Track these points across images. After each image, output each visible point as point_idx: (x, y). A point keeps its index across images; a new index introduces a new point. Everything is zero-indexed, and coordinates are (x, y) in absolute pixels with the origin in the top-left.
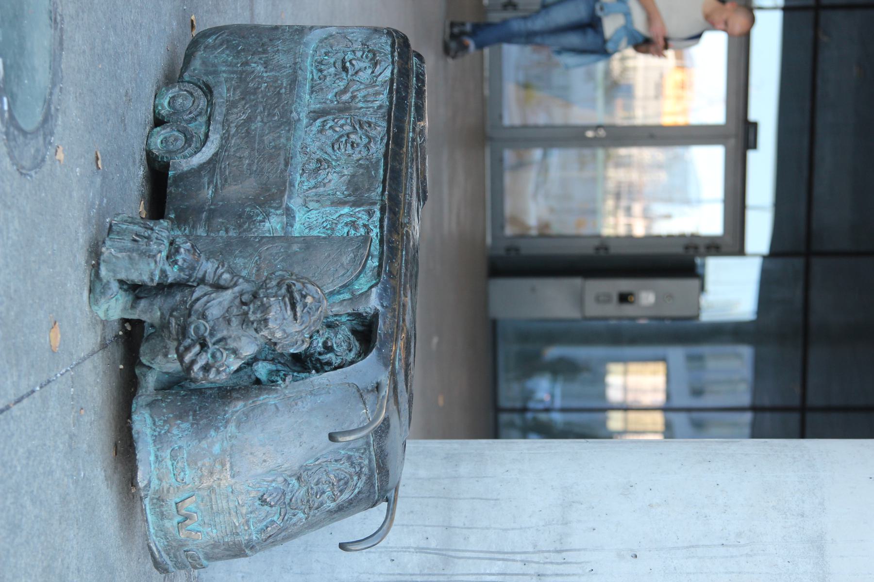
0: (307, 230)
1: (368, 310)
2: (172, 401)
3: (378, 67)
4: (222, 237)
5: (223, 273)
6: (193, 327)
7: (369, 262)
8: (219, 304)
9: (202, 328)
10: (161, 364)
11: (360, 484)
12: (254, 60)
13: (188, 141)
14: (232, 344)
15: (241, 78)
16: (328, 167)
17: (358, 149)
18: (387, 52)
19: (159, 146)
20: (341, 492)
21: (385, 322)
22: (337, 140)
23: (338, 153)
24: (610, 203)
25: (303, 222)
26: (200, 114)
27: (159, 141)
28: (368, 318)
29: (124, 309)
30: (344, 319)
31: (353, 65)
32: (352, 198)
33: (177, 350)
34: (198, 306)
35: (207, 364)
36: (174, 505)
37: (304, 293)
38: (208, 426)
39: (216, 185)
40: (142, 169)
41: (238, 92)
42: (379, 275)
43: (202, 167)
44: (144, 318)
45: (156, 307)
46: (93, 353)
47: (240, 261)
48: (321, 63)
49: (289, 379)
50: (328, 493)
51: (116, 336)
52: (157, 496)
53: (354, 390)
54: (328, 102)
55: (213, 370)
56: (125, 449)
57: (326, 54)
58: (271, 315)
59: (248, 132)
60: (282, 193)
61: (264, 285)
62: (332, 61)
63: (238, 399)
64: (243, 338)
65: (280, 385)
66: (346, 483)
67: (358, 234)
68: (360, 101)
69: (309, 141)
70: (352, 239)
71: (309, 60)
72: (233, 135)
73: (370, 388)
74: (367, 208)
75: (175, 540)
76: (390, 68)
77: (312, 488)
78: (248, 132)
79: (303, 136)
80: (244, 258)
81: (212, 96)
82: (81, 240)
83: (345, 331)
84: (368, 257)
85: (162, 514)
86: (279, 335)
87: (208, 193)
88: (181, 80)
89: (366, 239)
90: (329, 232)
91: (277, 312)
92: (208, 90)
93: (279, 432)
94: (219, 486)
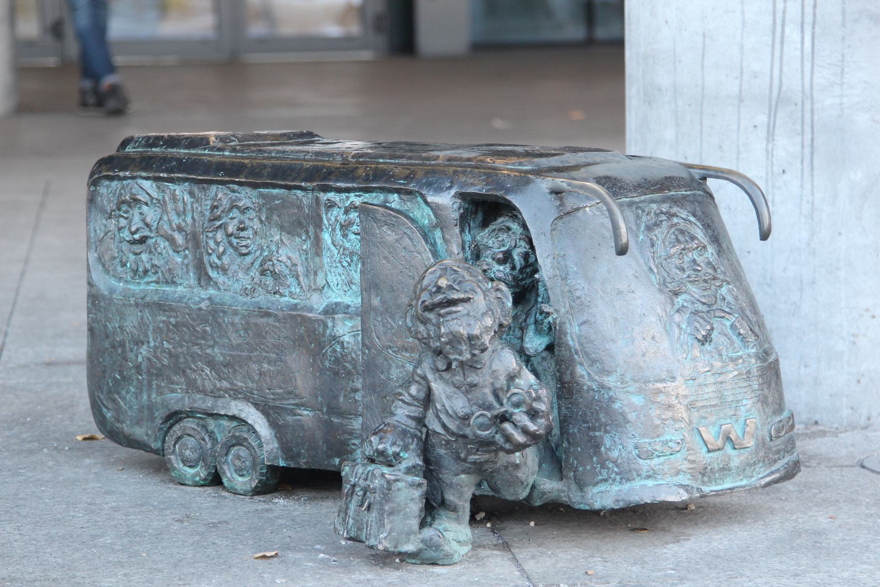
0: (354, 287)
1: (456, 206)
3: (139, 197)
4: (363, 397)
5: (410, 395)
6: (479, 432)
8: (450, 399)
9: (481, 420)
10: (529, 473)
11: (684, 214)
12: (134, 358)
13: (240, 442)
14: (502, 381)
15: (157, 375)
16: (270, 260)
17: (247, 222)
18: (119, 186)
20: (693, 238)
21: (472, 184)
22: (236, 249)
23: (253, 248)
25: (342, 293)
26: (204, 427)
27: (240, 479)
28: (467, 206)
29: (458, 520)
30: (468, 237)
32: (311, 229)
33: (509, 452)
34: (452, 426)
36: (711, 454)
37: (434, 290)
38: (608, 411)
39: (296, 405)
40: (276, 500)
41: (175, 378)
42: (410, 193)
43: (273, 424)
44: (468, 495)
45: (455, 480)
46: (515, 559)
48: (135, 272)
49: (546, 308)
50: (695, 255)
51: (493, 531)
52: (700, 476)
53: (560, 223)
54: (186, 261)
55: (535, 405)
56: (639, 518)
57: (124, 265)
58: (464, 331)
59: (227, 365)
60: (305, 320)
61: (424, 341)
62: (132, 257)
63: (573, 374)
64: (494, 367)
65: (555, 319)
66: (682, 232)
67: (358, 220)
68: (184, 220)
69: (237, 286)
70: (364, 229)
71: (132, 287)
72: (232, 384)
73: (558, 203)
74: (323, 209)
75: (756, 452)
76: (140, 181)
77: (689, 277)
78: (227, 365)
79: (230, 294)
83: (484, 237)
84: (387, 208)
85: (723, 469)
86: (489, 321)
88: (161, 452)
89: (364, 210)
90: (355, 258)
91: (460, 323)
93: (616, 320)
94: (686, 396)
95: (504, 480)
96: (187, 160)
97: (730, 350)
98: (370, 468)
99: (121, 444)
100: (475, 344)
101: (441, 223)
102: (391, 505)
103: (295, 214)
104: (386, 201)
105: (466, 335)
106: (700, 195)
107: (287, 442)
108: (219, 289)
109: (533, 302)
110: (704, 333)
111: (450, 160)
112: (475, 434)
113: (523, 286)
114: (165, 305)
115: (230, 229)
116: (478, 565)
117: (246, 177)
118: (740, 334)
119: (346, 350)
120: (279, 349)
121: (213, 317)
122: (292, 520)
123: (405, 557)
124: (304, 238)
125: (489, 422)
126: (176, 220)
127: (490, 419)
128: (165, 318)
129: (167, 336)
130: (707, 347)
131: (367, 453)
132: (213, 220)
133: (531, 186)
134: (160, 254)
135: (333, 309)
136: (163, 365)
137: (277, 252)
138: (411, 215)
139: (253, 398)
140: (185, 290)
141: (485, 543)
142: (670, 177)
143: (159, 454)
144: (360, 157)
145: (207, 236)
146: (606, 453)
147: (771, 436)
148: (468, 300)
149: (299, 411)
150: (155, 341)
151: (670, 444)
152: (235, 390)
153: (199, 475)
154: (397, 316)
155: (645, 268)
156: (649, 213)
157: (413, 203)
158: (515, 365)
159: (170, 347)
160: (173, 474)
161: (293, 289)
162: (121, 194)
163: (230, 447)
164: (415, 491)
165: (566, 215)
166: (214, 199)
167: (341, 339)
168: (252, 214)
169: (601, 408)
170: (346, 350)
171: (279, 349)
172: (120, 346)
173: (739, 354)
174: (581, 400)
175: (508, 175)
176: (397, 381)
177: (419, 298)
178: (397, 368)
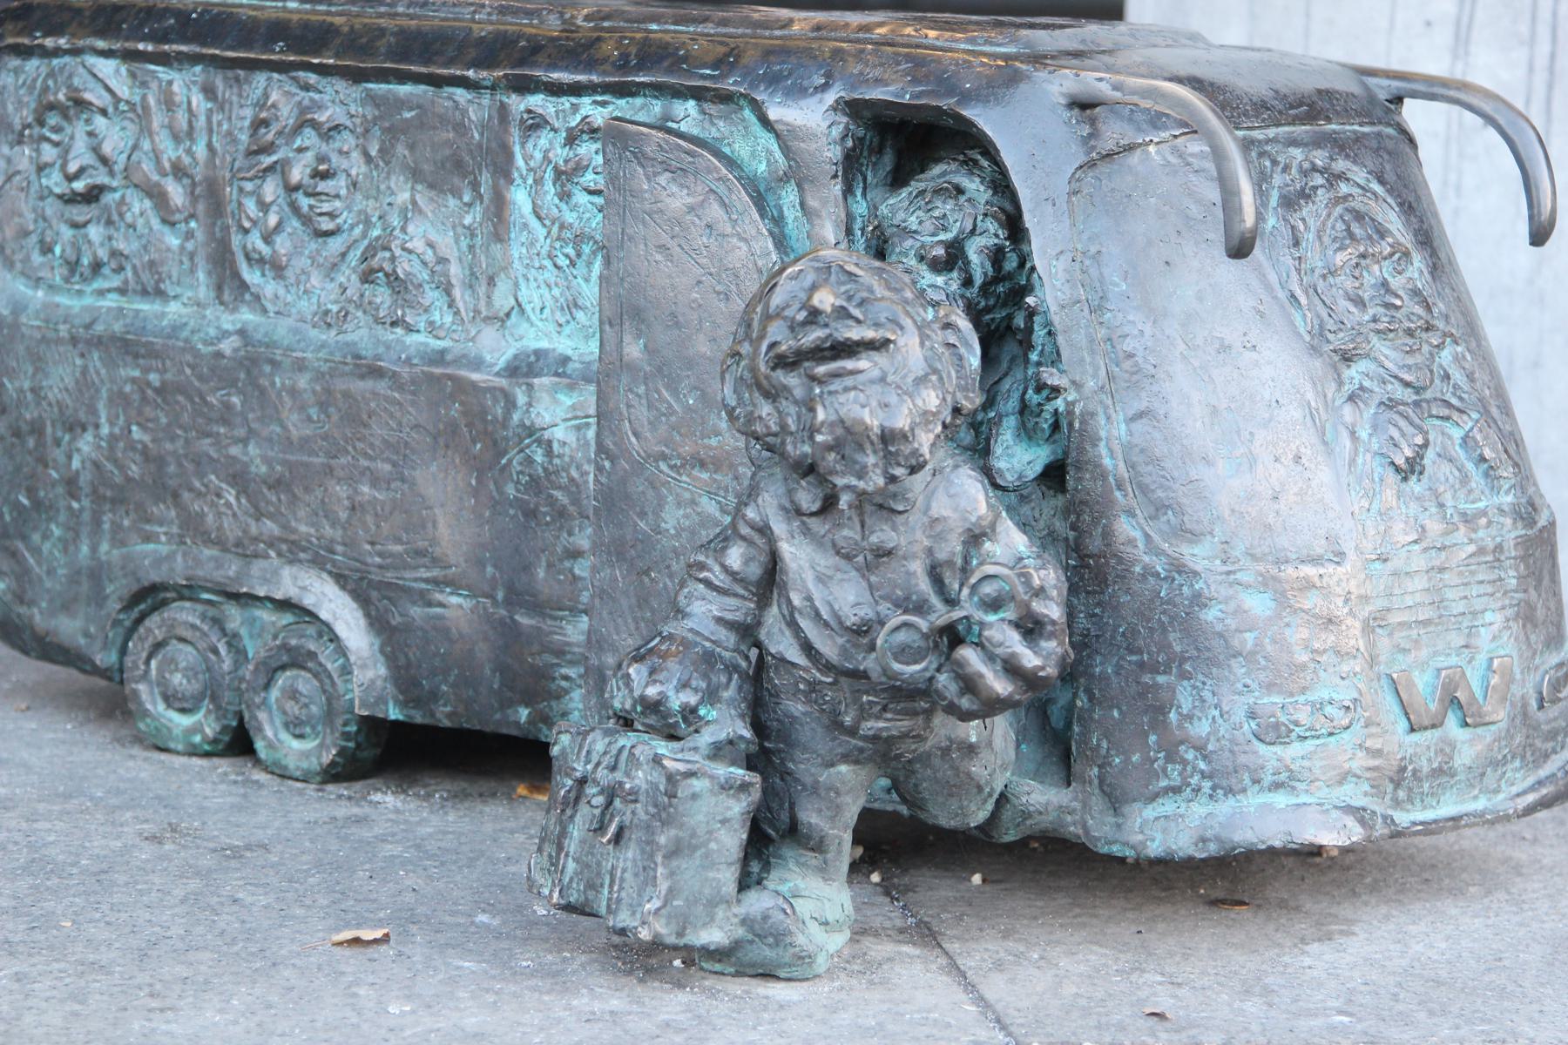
0: (580, 315)
1: (836, 132)
2: (1107, 735)
3: (88, 96)
4: (595, 570)
5: (726, 569)
6: (897, 666)
7: (683, 127)
9: (902, 637)
10: (995, 764)
11: (1359, 175)
12: (62, 459)
13: (297, 659)
14: (952, 547)
15: (113, 501)
16: (387, 248)
17: (335, 158)
18: (44, 70)
19: (309, 745)
20: (1382, 233)
21: (879, 82)
22: (306, 220)
23: (345, 218)
24: (22, 610)
25: (552, 327)
26: (218, 623)
27: (296, 744)
28: (861, 132)
29: (824, 871)
30: (860, 207)
31: (81, 171)
32: (485, 179)
33: (966, 716)
34: (829, 648)
35: (1017, 625)
36: (1416, 737)
38: (1188, 623)
39: (435, 582)
40: (377, 797)
41: (157, 510)
42: (726, 98)
43: (378, 624)
44: (851, 814)
47: (671, 518)
48: (73, 266)
49: (1052, 377)
50: (1385, 270)
51: (887, 893)
52: (1390, 788)
53: (1089, 178)
54: (190, 246)
55: (1038, 606)
56: (1231, 881)
57: (47, 249)
58: (872, 420)
59: (277, 484)
60: (463, 387)
62: (67, 233)
63: (1107, 534)
66: (1359, 216)
67: (599, 159)
68: (189, 151)
69: (306, 306)
70: (612, 179)
71: (63, 300)
72: (285, 527)
73: (1086, 130)
74: (515, 134)
75: (1509, 735)
76: (91, 60)
77: (1375, 320)
78: (277, 484)
79: (290, 321)
80: (661, 505)
81: (163, 587)
82: (615, 1003)
83: (898, 207)
84: (669, 131)
85: (1438, 772)
86: (931, 399)
87: (456, 604)
88: (116, 676)
89: (615, 136)
91: (870, 398)
92: (149, 597)
93: (1214, 411)
94: (1365, 599)
95: (937, 781)
96: (201, 14)
97: (1461, 494)
98: (626, 740)
99: (26, 652)
100: (897, 453)
101: (797, 173)
102: (673, 832)
103: (448, 143)
104: (667, 117)
105: (877, 430)
106: (1389, 137)
107: (409, 665)
108: (265, 311)
109: (1005, 365)
110: (1409, 453)
111: (818, 28)
112: (885, 671)
113: (988, 325)
114: (137, 343)
115: (297, 174)
116: (871, 982)
117: (337, 56)
118: (1483, 459)
119: (557, 461)
120: (400, 452)
121: (248, 372)
122: (418, 847)
123: (698, 959)
124: (466, 199)
125: (922, 644)
126: (170, 151)
127: (925, 636)
128: (137, 373)
129: (140, 413)
130: (1415, 486)
131: (617, 705)
132: (256, 153)
133: (1023, 86)
134: (132, 226)
135: (530, 365)
136: (129, 480)
137: (404, 230)
138: (727, 150)
139: (334, 562)
140: (184, 311)
141: (877, 922)
142: (1328, 92)
143: (110, 679)
144: (604, 19)
145: (241, 190)
146: (1180, 727)
147: (1542, 699)
148: (884, 344)
149: (439, 597)
150: (112, 424)
151: (1329, 710)
152: (293, 542)
153: (202, 731)
154: (684, 386)
155: (1282, 295)
156: (1286, 169)
157: (733, 123)
158: (983, 509)
159: (146, 438)
160: (142, 726)
161: (436, 317)
162: (46, 89)
163: (275, 670)
164: (731, 802)
165: (1099, 160)
166: (261, 105)
167: (547, 435)
168: (347, 141)
169: (1172, 619)
170: (557, 461)
171: (400, 452)
172: (32, 432)
173: (1481, 505)
174: (1125, 598)
175: (965, 61)
176: (678, 535)
177: (762, 337)
178: (679, 505)
